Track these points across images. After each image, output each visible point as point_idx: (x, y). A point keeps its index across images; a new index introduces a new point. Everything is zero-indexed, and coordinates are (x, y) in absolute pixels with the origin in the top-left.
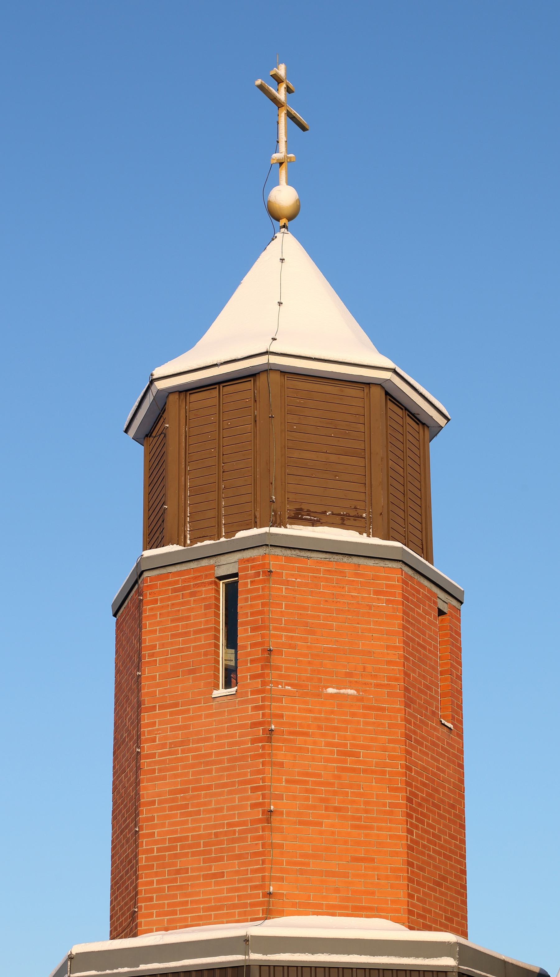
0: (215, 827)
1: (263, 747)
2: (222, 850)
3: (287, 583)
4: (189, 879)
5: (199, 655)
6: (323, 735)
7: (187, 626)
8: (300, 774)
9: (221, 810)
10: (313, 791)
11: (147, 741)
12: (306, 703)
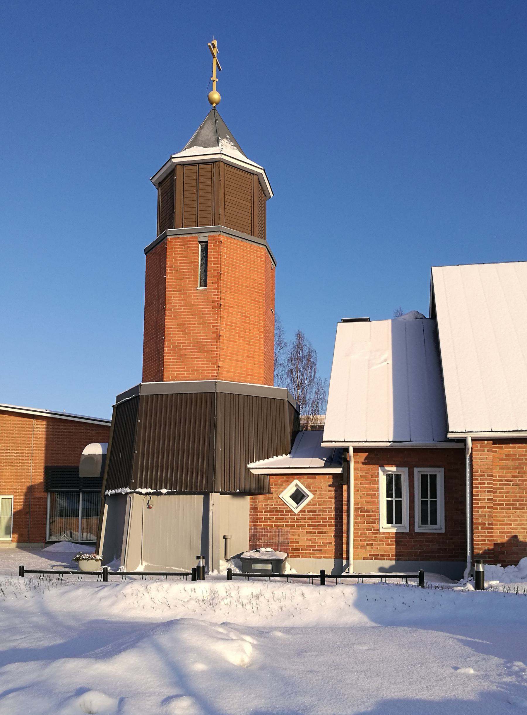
0: (197, 339)
1: (217, 310)
2: (200, 349)
3: (227, 247)
4: (186, 358)
5: (191, 272)
6: (238, 309)
7: (186, 260)
8: (230, 322)
9: (199, 333)
10: (234, 329)
11: (168, 303)
12: (232, 295)
